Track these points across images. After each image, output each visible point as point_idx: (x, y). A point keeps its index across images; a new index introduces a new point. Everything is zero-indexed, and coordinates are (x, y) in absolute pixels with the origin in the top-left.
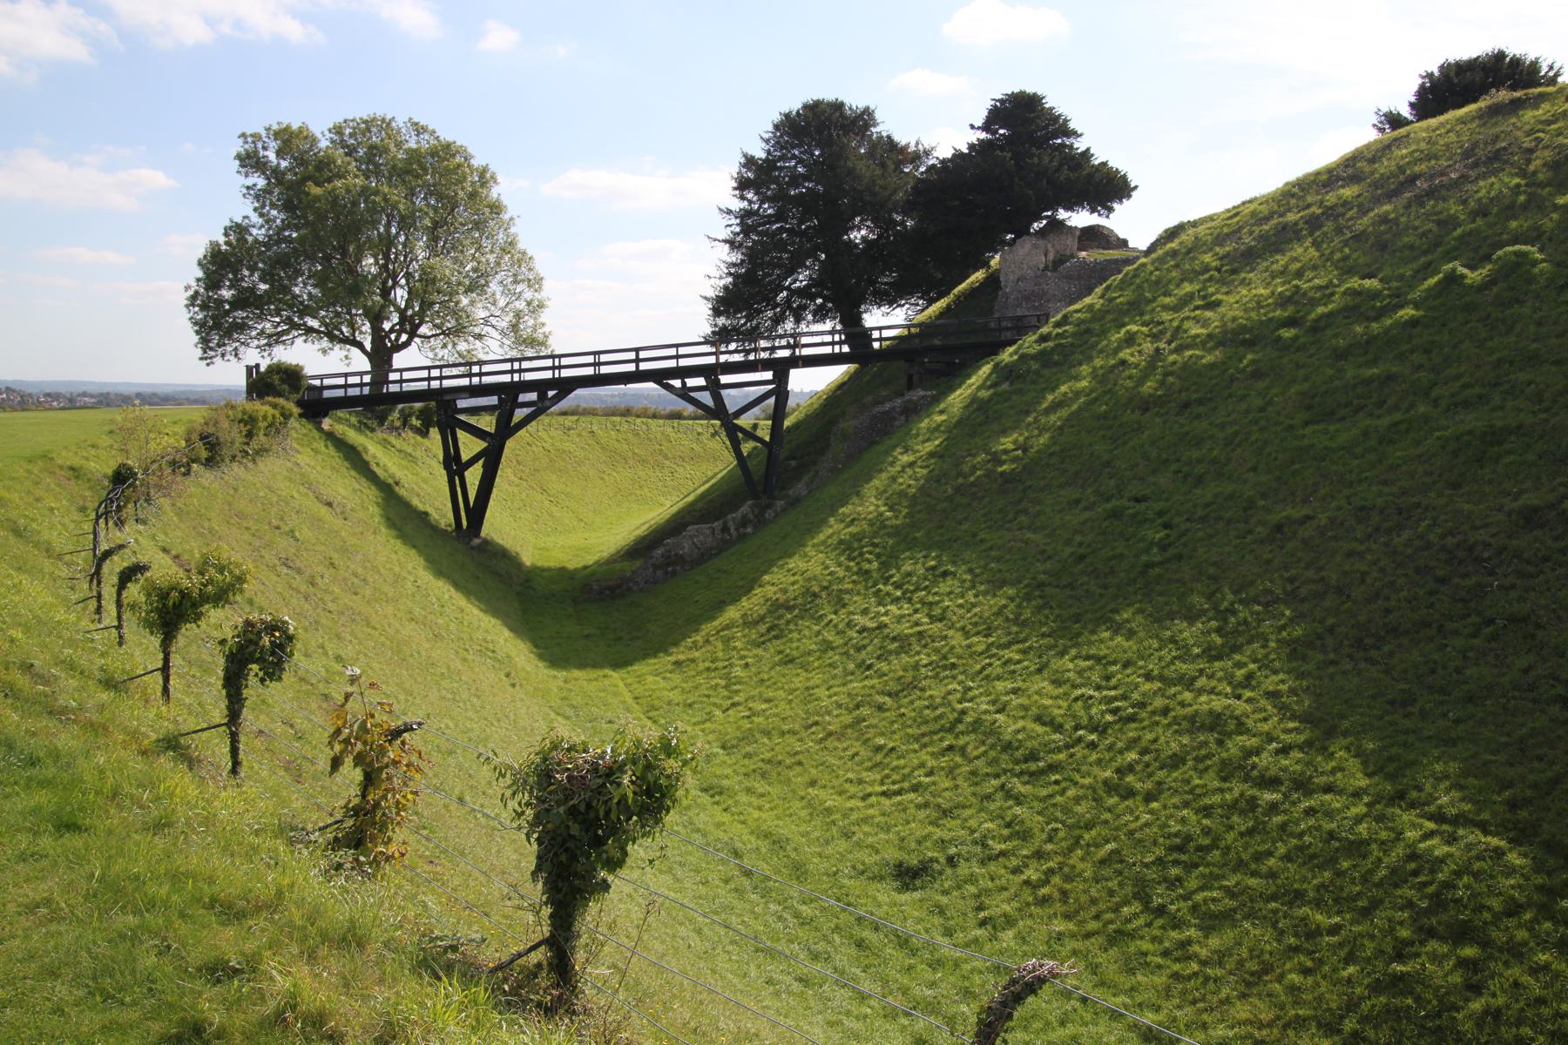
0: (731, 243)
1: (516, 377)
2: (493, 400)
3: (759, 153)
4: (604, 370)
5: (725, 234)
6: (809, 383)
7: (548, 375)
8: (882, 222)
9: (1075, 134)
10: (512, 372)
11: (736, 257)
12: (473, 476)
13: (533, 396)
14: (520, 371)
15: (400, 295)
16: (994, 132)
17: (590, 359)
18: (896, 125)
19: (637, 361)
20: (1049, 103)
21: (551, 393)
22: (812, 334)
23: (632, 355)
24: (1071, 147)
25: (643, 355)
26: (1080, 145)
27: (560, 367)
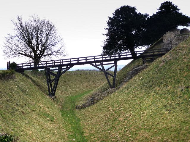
0: (107, 35)
1: (62, 63)
2: (57, 68)
3: (112, 16)
4: (80, 61)
5: (106, 33)
6: (122, 64)
7: (68, 63)
8: (139, 30)
9: (178, 9)
10: (69, 61)
11: (108, 38)
12: (53, 83)
13: (65, 67)
14: (71, 61)
15: (40, 47)
16: (162, 10)
17: (76, 59)
18: (141, 10)
19: (94, 59)
20: (173, 3)
21: (69, 66)
22: (123, 53)
23: (93, 58)
24: (178, 12)
25: (95, 57)
26: (180, 12)
27: (79, 60)
